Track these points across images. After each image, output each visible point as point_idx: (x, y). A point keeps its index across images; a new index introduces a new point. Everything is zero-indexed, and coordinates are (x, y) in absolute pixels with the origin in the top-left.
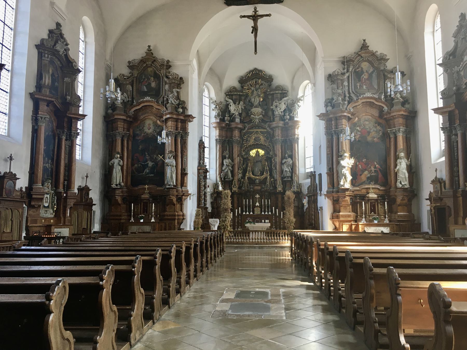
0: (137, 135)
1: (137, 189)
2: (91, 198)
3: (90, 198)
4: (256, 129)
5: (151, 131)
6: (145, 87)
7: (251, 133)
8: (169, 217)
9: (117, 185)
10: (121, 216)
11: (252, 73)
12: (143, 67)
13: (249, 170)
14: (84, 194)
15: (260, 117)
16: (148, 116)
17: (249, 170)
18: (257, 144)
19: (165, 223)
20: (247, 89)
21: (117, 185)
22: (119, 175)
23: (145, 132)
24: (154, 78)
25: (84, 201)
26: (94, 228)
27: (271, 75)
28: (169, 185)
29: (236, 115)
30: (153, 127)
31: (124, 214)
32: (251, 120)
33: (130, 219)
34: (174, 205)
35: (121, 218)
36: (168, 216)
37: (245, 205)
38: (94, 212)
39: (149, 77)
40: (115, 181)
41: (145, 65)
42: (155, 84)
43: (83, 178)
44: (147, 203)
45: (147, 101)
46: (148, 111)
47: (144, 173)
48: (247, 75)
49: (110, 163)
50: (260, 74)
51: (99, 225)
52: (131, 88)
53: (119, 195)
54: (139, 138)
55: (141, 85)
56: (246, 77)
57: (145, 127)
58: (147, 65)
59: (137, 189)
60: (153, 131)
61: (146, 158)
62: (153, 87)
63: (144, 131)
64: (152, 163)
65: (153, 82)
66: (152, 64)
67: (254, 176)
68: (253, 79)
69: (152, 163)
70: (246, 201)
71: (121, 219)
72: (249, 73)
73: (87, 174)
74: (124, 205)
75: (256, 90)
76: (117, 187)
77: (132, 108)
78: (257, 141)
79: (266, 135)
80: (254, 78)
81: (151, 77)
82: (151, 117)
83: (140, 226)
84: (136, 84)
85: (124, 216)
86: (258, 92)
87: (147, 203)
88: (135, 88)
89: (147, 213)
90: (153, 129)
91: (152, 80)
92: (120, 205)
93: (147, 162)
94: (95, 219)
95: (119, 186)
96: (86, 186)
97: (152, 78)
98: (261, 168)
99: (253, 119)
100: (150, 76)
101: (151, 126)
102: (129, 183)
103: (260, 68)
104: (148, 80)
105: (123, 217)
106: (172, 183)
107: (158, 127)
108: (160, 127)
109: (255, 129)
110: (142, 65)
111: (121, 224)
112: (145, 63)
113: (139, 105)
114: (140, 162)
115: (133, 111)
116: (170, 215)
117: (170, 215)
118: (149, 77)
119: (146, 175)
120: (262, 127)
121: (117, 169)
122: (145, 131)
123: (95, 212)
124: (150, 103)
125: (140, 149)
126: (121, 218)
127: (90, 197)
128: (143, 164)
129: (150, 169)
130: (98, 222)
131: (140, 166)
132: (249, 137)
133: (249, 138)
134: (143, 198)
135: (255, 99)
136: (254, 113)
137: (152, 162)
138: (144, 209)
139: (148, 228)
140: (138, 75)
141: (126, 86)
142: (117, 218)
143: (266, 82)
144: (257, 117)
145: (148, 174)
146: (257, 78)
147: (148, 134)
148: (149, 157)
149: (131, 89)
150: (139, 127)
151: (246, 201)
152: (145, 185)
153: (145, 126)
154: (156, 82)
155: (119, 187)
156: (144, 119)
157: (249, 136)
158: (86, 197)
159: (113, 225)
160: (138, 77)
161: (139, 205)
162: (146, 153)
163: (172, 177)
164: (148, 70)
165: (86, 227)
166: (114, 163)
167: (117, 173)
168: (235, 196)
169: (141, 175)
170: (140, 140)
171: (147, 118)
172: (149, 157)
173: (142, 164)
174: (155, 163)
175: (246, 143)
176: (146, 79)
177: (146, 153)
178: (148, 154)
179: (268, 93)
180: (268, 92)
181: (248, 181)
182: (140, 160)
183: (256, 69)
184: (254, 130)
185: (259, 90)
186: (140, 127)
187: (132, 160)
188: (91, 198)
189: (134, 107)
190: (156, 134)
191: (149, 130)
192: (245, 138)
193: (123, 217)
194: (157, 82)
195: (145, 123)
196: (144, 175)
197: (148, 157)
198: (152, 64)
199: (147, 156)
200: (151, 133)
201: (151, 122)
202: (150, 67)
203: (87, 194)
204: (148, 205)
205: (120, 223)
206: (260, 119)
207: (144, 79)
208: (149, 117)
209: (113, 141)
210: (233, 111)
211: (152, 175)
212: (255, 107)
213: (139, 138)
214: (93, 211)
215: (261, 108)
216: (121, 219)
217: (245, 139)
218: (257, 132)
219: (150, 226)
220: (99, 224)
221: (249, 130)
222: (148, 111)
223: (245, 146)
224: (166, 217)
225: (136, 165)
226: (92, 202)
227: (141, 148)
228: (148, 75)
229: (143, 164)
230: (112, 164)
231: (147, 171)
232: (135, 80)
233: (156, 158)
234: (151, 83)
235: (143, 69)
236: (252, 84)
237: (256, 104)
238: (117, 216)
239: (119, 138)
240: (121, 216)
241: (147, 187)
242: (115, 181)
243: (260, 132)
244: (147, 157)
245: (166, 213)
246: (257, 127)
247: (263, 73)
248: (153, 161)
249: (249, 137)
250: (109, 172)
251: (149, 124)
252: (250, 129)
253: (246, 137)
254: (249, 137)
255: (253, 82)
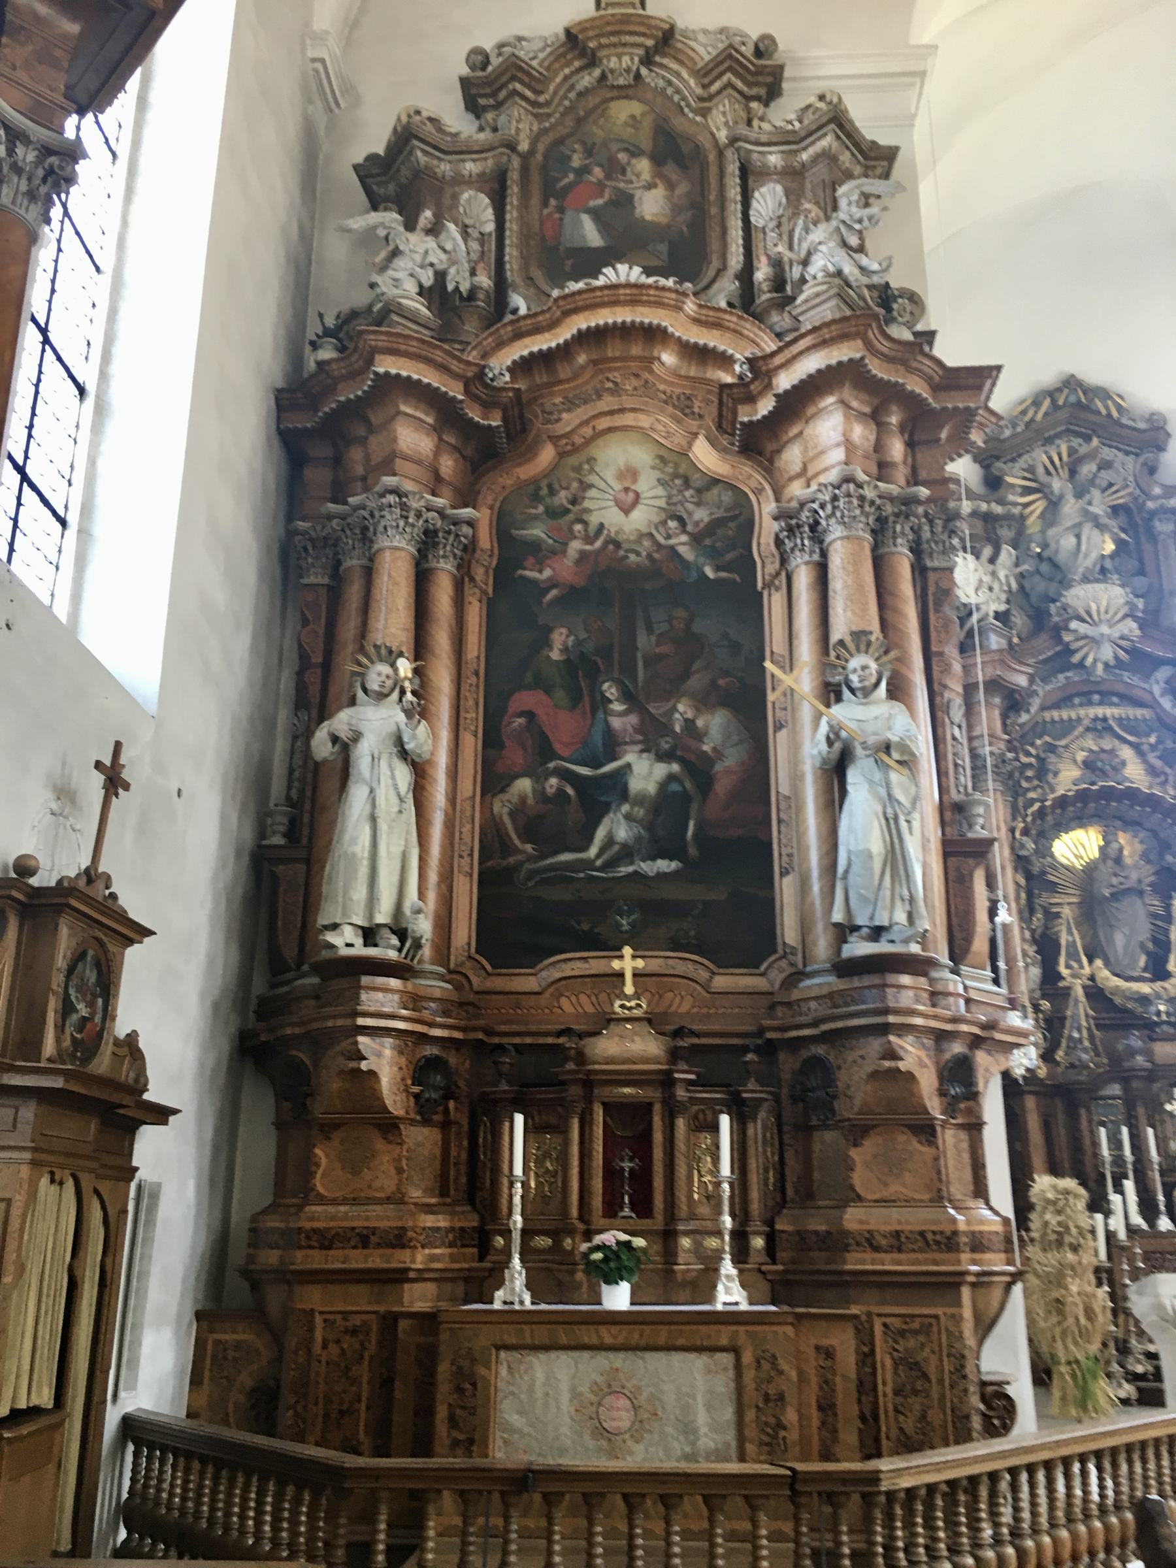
0: (535, 548)
1: (530, 983)
2: (132, 1037)
3: (117, 1043)
4: (1090, 703)
5: (640, 519)
6: (586, 220)
7: (1067, 727)
8: (888, 1263)
9: (369, 935)
10: (399, 1239)
11: (1054, 402)
12: (572, 95)
13: (1072, 945)
14: (61, 962)
15: (1126, 632)
16: (622, 411)
17: (1072, 945)
18: (1107, 794)
19: (864, 1335)
20: (1023, 487)
21: (369, 935)
22: (397, 850)
23: (592, 529)
24: (658, 161)
25: (49, 1046)
26: (132, 1387)
27: (1160, 414)
28: (877, 932)
29: (987, 615)
30: (660, 491)
31: (429, 1221)
32: (1068, 651)
33: (496, 1276)
34: (926, 1130)
35: (401, 1258)
36: (877, 1249)
37: (1135, 1163)
38: (150, 1196)
39: (622, 157)
40: (359, 893)
41: (587, 80)
42: (666, 197)
43: (65, 794)
44: (646, 1109)
45: (614, 295)
46: (617, 376)
47: (593, 851)
48: (1024, 412)
49: (321, 736)
50: (1099, 413)
51: (177, 1333)
52: (489, 214)
53: (387, 1031)
54: (547, 573)
55: (561, 210)
56: (1014, 426)
57: (592, 493)
58: (603, 77)
59: (530, 983)
60: (664, 523)
61: (608, 730)
62: (651, 223)
63: (585, 523)
64: (661, 770)
65: (650, 186)
66: (644, 71)
67: (1117, 982)
68: (1049, 441)
69: (661, 770)
70: (1115, 1143)
71: (399, 1277)
72: (1036, 403)
73: (118, 746)
74: (426, 1131)
75: (1079, 495)
76: (372, 952)
77: (501, 344)
78: (1103, 771)
79: (1152, 740)
80: (1058, 436)
81: (636, 153)
82: (644, 421)
83: (619, 1360)
84: (525, 195)
85: (431, 1237)
86: (1090, 503)
87: (646, 1109)
88: (511, 214)
89: (643, 1207)
90: (662, 503)
91: (646, 176)
92: (389, 1126)
93: (614, 758)
94: (144, 1274)
95: (395, 941)
96: (91, 875)
97: (643, 166)
98: (1144, 932)
99: (1081, 643)
100: (626, 150)
101: (648, 485)
102: (463, 933)
103: (1093, 375)
104: (608, 176)
105: (419, 1259)
106: (901, 917)
107: (699, 491)
108: (715, 491)
109: (1081, 705)
110: (566, 78)
111: (403, 1324)
112: (592, 61)
113: (553, 325)
114: (554, 756)
115: (509, 369)
116: (897, 1234)
117: (898, 1241)
118: (622, 157)
119: (610, 865)
120: (1122, 697)
121: (381, 794)
122: (594, 520)
123: (155, 1196)
124: (645, 310)
125: (555, 655)
126: (401, 1258)
127: (121, 1029)
128: (584, 771)
129: (640, 812)
130: (173, 1310)
131: (561, 792)
132: (1052, 752)
133: (1052, 759)
134: (610, 1060)
135: (1078, 536)
136: (1089, 613)
137: (662, 757)
138: (611, 1174)
139: (700, 1382)
140: (541, 148)
141: (455, 197)
142: (359, 1260)
143: (1127, 453)
144: (1105, 629)
145: (627, 853)
146: (1078, 434)
147: (618, 545)
148: (633, 719)
149: (490, 227)
150: (544, 491)
151: (1115, 1143)
152: (614, 948)
153: (591, 486)
154: (671, 186)
155: (392, 955)
156: (587, 431)
157: (1056, 746)
158: (83, 1009)
159: (318, 1335)
160: (539, 157)
161: (564, 1131)
162: (610, 690)
163: (895, 858)
164: (612, 112)
165: (44, 1397)
166: (357, 736)
167: (383, 826)
168: (1030, 1103)
169: (568, 866)
170: (552, 584)
171: (610, 430)
172: (633, 719)
173: (567, 776)
174: (682, 761)
175: (1034, 789)
176: (597, 171)
177: (610, 690)
178: (627, 696)
179: (1151, 505)
180: (1154, 498)
181: (1091, 1013)
182: (557, 747)
183: (1071, 383)
184: (1082, 712)
185: (1096, 494)
186: (552, 492)
187: (492, 740)
188: (132, 1037)
189: (518, 336)
190: (684, 538)
191: (627, 511)
192: (1028, 754)
193: (419, 1259)
194: (683, 188)
195: (591, 460)
196: (588, 864)
197: (621, 719)
198: (644, 71)
199: (617, 707)
200: (641, 536)
201: (640, 456)
202: (624, 93)
203: (92, 976)
204: (658, 1136)
205: (390, 1321)
206: (1123, 643)
207: (584, 170)
208: (628, 419)
209: (335, 592)
210: (971, 593)
211: (664, 865)
212: (1086, 579)
213: (547, 573)
214: (139, 1188)
215: (1122, 586)
216: (399, 1277)
217: (1030, 765)
218: (1101, 727)
219: (726, 1359)
220: (178, 1322)
221: (1047, 715)
222: (617, 376)
223: (1033, 802)
224: (858, 1261)
225: (524, 785)
226: (141, 1085)
227: (565, 650)
228: (614, 147)
229: (584, 771)
230: (335, 739)
231: (623, 833)
232: (514, 176)
233: (689, 724)
234: (638, 194)
235: (568, 111)
236: (1052, 462)
237: (1089, 563)
238: (364, 1239)
239: (399, 541)
240: (399, 1239)
241: (628, 962)
242: (359, 893)
243: (1120, 725)
244: (616, 723)
245: (853, 1218)
246: (1096, 697)
247: (1115, 402)
248: (665, 746)
249: (1052, 749)
250: (291, 834)
251: (631, 473)
252: (1057, 706)
253: (1033, 751)
254: (1052, 749)
255: (1060, 455)
